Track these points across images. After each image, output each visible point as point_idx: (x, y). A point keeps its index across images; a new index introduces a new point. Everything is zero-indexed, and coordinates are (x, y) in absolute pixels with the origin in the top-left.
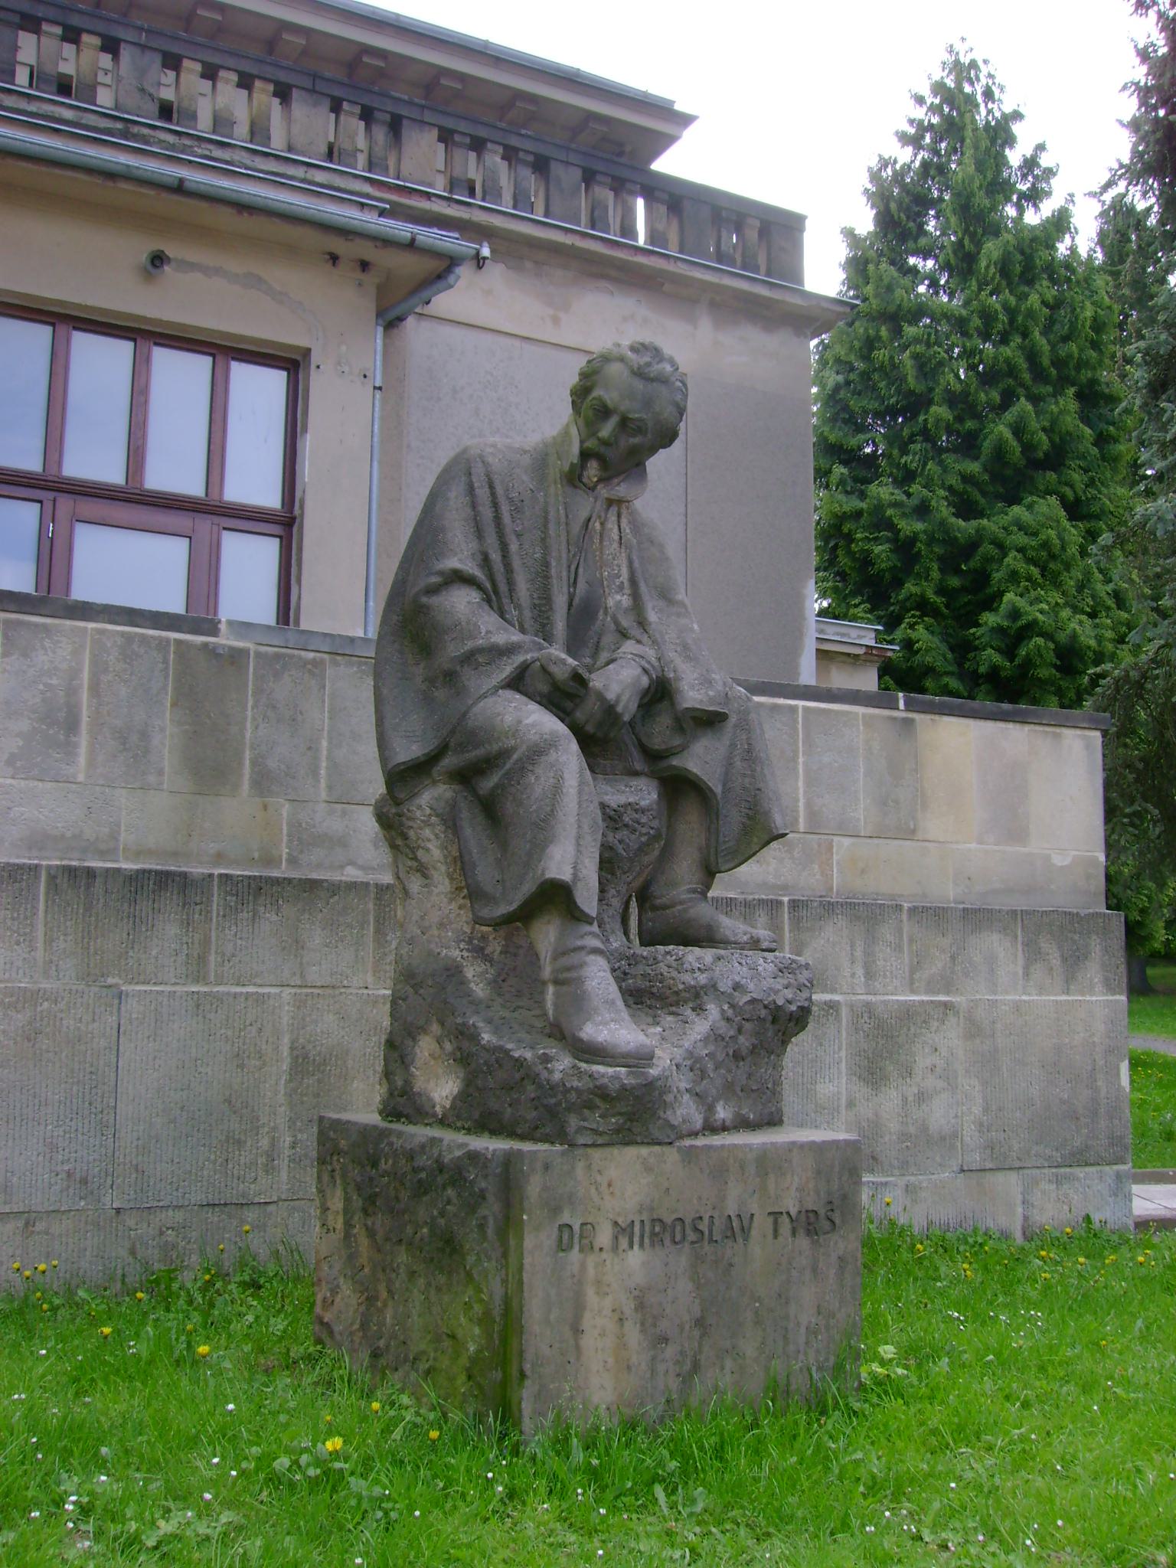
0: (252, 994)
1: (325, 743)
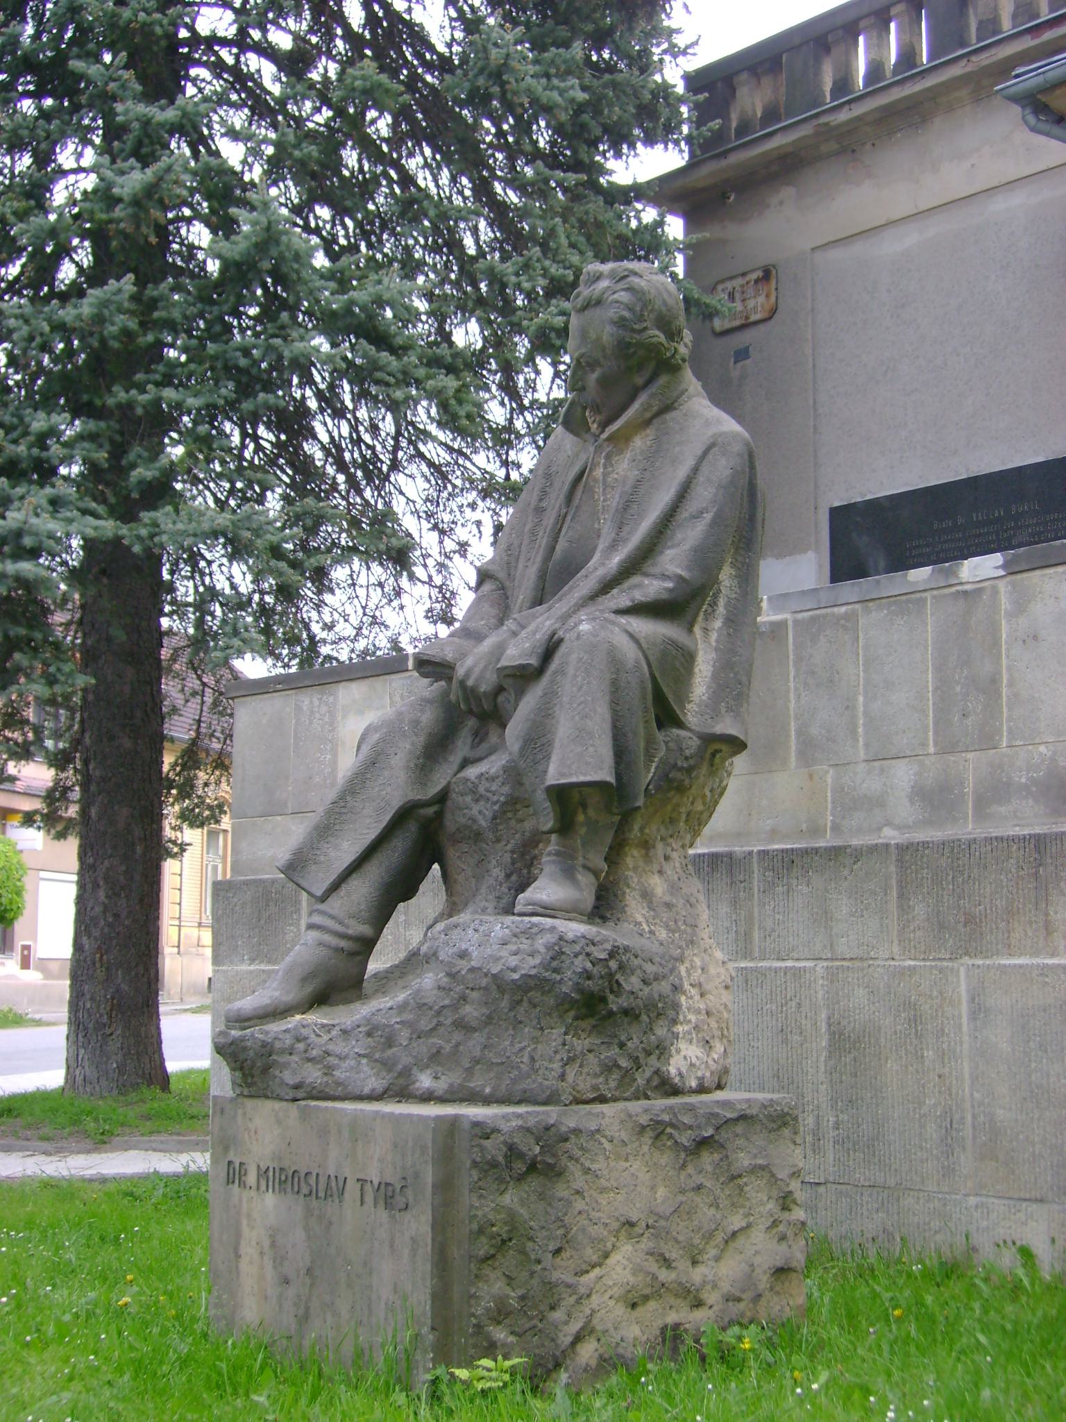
0: (791, 968)
1: (861, 699)
